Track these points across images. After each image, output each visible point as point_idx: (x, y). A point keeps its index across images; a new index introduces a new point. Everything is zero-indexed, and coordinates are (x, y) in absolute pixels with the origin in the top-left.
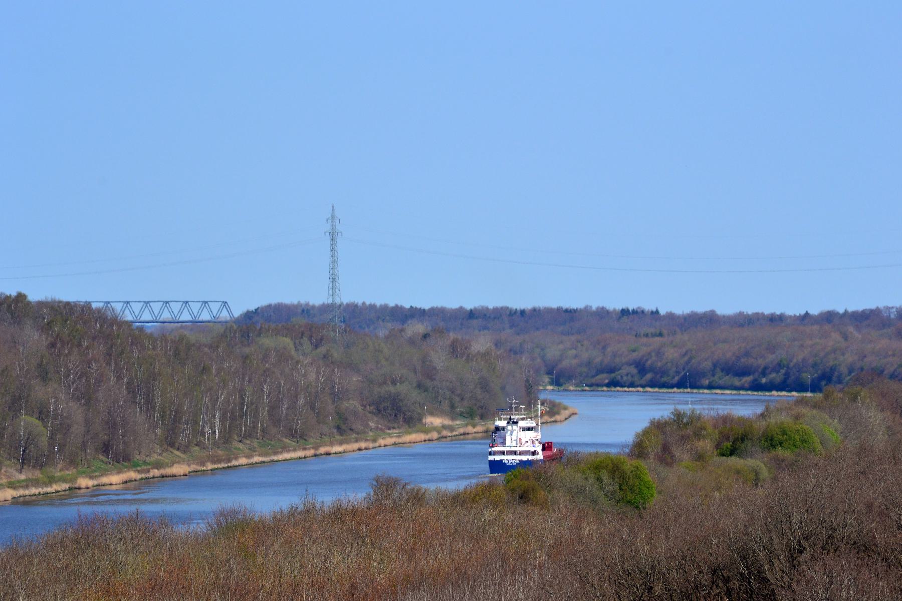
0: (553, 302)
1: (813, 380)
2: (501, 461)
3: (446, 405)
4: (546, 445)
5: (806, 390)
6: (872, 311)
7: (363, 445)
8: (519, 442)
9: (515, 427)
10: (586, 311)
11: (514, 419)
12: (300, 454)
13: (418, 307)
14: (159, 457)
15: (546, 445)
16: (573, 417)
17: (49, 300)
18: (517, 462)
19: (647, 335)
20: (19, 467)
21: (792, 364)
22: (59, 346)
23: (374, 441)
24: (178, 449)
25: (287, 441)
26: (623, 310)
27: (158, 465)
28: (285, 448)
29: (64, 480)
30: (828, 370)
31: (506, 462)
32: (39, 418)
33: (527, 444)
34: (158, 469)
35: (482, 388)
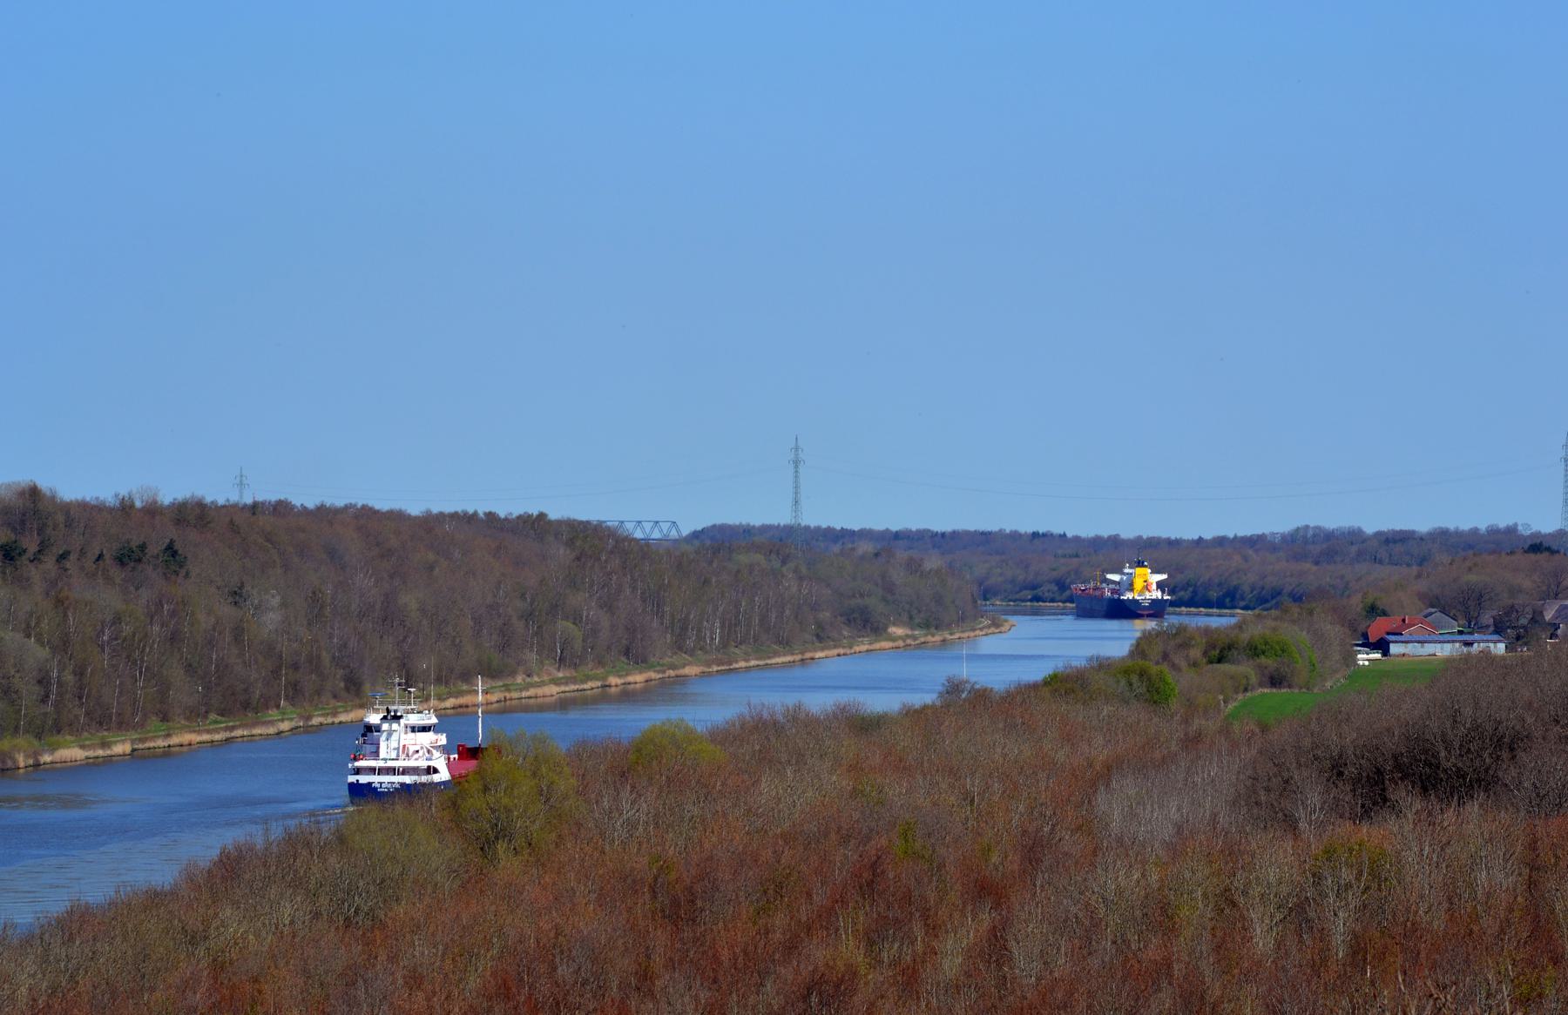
0: (971, 526)
1: (1218, 598)
2: (370, 784)
3: (905, 617)
5: (1212, 607)
7: (841, 651)
8: (404, 751)
9: (395, 726)
10: (1001, 533)
11: (395, 711)
13: (849, 528)
14: (670, 660)
16: (1013, 628)
17: (566, 519)
18: (398, 786)
21: (1199, 583)
23: (851, 648)
24: (685, 653)
25: (775, 647)
26: (1034, 533)
27: (673, 667)
28: (776, 654)
29: (595, 678)
32: (574, 623)
33: (416, 756)
34: (673, 670)
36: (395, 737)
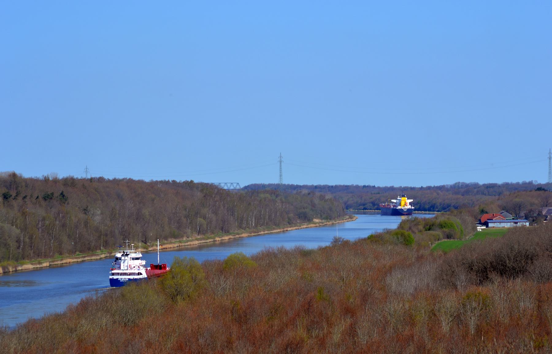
2: (117, 279)
3: (319, 216)
4: (162, 266)
6: (442, 186)
7: (297, 228)
9: (126, 258)
12: (279, 230)
13: (299, 185)
15: (162, 266)
18: (128, 279)
19: (374, 194)
20: (198, 234)
21: (422, 203)
22: (206, 196)
23: (300, 226)
24: (243, 229)
25: (274, 226)
27: (238, 234)
28: (274, 229)
29: (211, 238)
30: (433, 204)
31: (120, 279)
33: (134, 269)
35: (330, 210)
36: (126, 262)
